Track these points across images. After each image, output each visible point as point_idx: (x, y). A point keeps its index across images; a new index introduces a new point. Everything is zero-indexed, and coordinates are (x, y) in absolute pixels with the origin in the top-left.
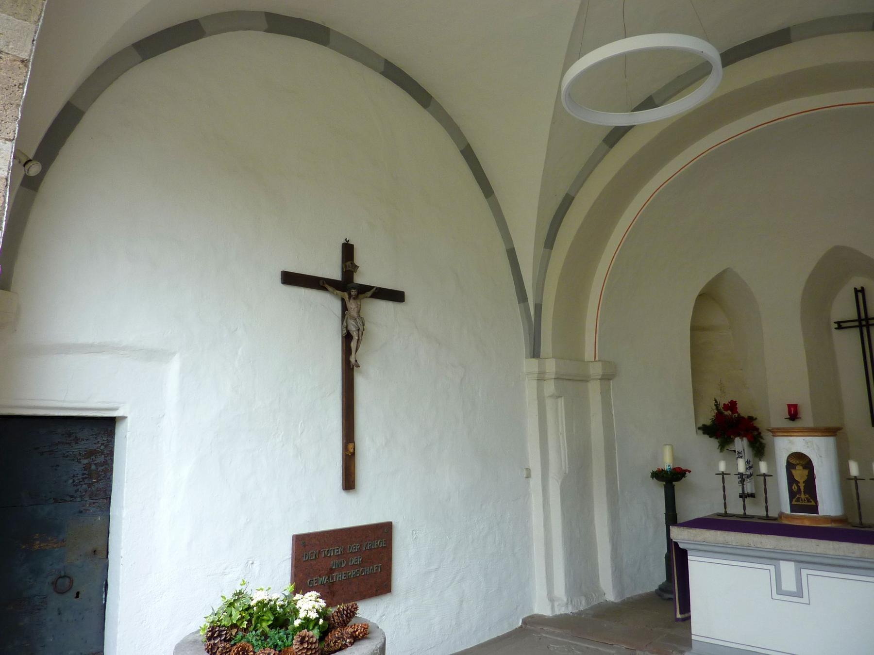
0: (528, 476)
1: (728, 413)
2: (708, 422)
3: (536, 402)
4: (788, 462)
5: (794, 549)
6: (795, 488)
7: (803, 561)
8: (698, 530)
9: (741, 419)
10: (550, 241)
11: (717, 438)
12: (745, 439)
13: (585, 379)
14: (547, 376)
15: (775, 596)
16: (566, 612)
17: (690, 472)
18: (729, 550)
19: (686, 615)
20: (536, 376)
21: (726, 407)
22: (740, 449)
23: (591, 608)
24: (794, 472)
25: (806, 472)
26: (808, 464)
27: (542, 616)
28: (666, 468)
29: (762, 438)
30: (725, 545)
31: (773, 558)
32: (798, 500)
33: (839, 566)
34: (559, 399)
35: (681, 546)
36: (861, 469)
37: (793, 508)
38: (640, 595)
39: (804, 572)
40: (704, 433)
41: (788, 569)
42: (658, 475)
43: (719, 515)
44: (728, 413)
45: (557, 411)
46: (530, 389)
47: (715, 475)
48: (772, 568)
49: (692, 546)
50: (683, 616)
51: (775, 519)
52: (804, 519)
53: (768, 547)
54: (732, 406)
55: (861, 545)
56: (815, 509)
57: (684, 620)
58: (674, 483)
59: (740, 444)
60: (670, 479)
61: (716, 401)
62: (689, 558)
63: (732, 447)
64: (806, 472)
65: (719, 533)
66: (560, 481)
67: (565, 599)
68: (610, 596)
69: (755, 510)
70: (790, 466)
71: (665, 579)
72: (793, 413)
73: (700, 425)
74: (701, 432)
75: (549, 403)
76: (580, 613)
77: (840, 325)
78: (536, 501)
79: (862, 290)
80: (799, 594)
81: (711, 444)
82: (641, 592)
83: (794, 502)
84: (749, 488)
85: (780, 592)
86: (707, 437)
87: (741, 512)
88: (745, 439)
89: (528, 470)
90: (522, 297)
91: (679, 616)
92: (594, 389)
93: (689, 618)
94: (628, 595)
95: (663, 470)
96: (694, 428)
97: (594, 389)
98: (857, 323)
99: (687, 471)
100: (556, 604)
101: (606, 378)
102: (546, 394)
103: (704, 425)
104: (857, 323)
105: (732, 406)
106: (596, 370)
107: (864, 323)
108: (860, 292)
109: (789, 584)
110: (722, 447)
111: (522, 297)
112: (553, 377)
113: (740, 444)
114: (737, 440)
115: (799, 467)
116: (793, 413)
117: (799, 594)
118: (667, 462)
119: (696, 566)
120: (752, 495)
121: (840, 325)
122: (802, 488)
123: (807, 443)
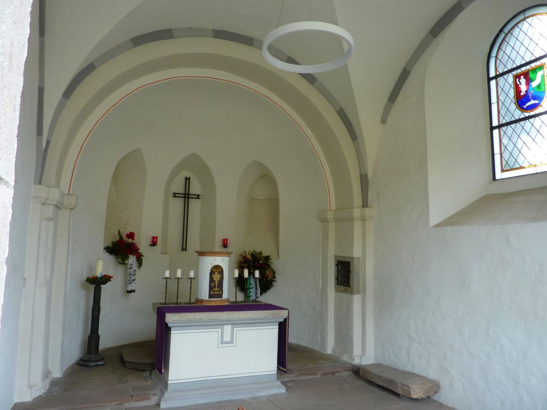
4: (211, 271)
5: (257, 317)
6: (213, 285)
7: (235, 324)
10: (68, 93)
12: (135, 256)
15: (234, 344)
24: (214, 276)
25: (220, 276)
26: (221, 272)
28: (99, 275)
31: (220, 324)
32: (213, 292)
33: (255, 323)
36: (195, 275)
37: (211, 296)
39: (235, 329)
40: (107, 252)
41: (227, 328)
48: (220, 330)
52: (216, 302)
54: (131, 235)
55: (266, 311)
56: (221, 296)
58: (101, 286)
60: (97, 283)
61: (119, 232)
62: (172, 332)
64: (220, 276)
65: (197, 314)
70: (212, 273)
72: (225, 244)
73: (105, 246)
74: (105, 251)
77: (198, 197)
79: (189, 179)
80: (232, 342)
83: (211, 293)
85: (222, 342)
86: (108, 254)
87: (234, 300)
90: (39, 132)
92: (332, 227)
98: (190, 196)
103: (108, 247)
104: (183, 196)
105: (131, 235)
107: (187, 196)
108: (187, 179)
109: (227, 338)
111: (39, 132)
113: (132, 260)
115: (216, 273)
116: (154, 242)
117: (232, 342)
118: (99, 272)
121: (198, 197)
122: (216, 285)
123: (222, 260)
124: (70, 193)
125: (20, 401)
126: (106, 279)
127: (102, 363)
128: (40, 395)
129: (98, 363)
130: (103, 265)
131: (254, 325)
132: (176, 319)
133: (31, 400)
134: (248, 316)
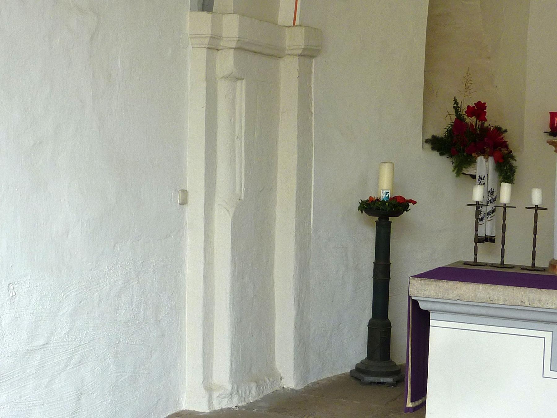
0: (184, 203)
1: (472, 120)
2: (441, 132)
3: (204, 85)
8: (451, 283)
9: (485, 131)
11: (451, 156)
12: (491, 159)
13: (275, 54)
14: (223, 43)
15: (548, 373)
16: (230, 406)
17: (414, 203)
18: (491, 312)
19: (420, 401)
20: (207, 41)
21: (471, 111)
22: (484, 174)
23: (264, 399)
27: (194, 412)
28: (382, 196)
29: (513, 158)
30: (489, 304)
34: (239, 83)
35: (423, 306)
36: (544, 198)
38: (329, 379)
40: (433, 149)
42: (370, 207)
43: (466, 263)
44: (472, 120)
45: (234, 102)
46: (195, 61)
47: (445, 210)
49: (438, 307)
50: (417, 403)
51: (544, 270)
53: (549, 306)
54: (479, 110)
57: (415, 409)
58: (391, 219)
59: (484, 165)
60: (385, 213)
61: (456, 103)
62: (432, 322)
63: (471, 171)
65: (481, 286)
66: (232, 211)
67: (229, 387)
68: (290, 381)
69: (488, 257)
71: (364, 356)
73: (429, 137)
74: (428, 146)
75: (222, 87)
76: (250, 406)
78: (193, 241)
81: (443, 164)
82: (329, 375)
84: (488, 228)
86: (436, 154)
88: (491, 159)
89: (184, 192)
91: (409, 405)
92: (288, 70)
93: (424, 404)
94: (313, 379)
95: (378, 200)
96: (420, 140)
97: (288, 70)
99: (411, 201)
100: (215, 394)
101: (309, 54)
102: (219, 73)
103: (434, 137)
105: (479, 110)
106: (295, 40)
110: (459, 170)
112: (234, 45)
113: (484, 165)
114: (481, 159)
118: (384, 189)
119: (439, 333)
120: (491, 240)
124: (297, 23)
125: (191, 409)
126: (397, 206)
127: (389, 380)
128: (229, 409)
129: (382, 380)
130: (430, 182)
131: (460, 317)
132: (433, 293)
133: (207, 411)
134: (452, 295)
